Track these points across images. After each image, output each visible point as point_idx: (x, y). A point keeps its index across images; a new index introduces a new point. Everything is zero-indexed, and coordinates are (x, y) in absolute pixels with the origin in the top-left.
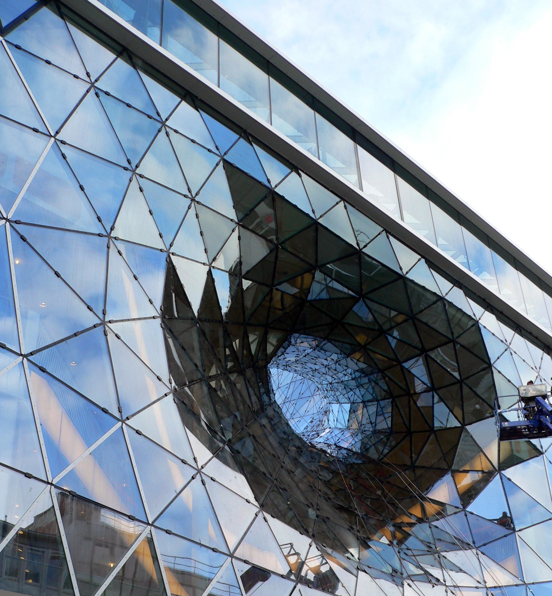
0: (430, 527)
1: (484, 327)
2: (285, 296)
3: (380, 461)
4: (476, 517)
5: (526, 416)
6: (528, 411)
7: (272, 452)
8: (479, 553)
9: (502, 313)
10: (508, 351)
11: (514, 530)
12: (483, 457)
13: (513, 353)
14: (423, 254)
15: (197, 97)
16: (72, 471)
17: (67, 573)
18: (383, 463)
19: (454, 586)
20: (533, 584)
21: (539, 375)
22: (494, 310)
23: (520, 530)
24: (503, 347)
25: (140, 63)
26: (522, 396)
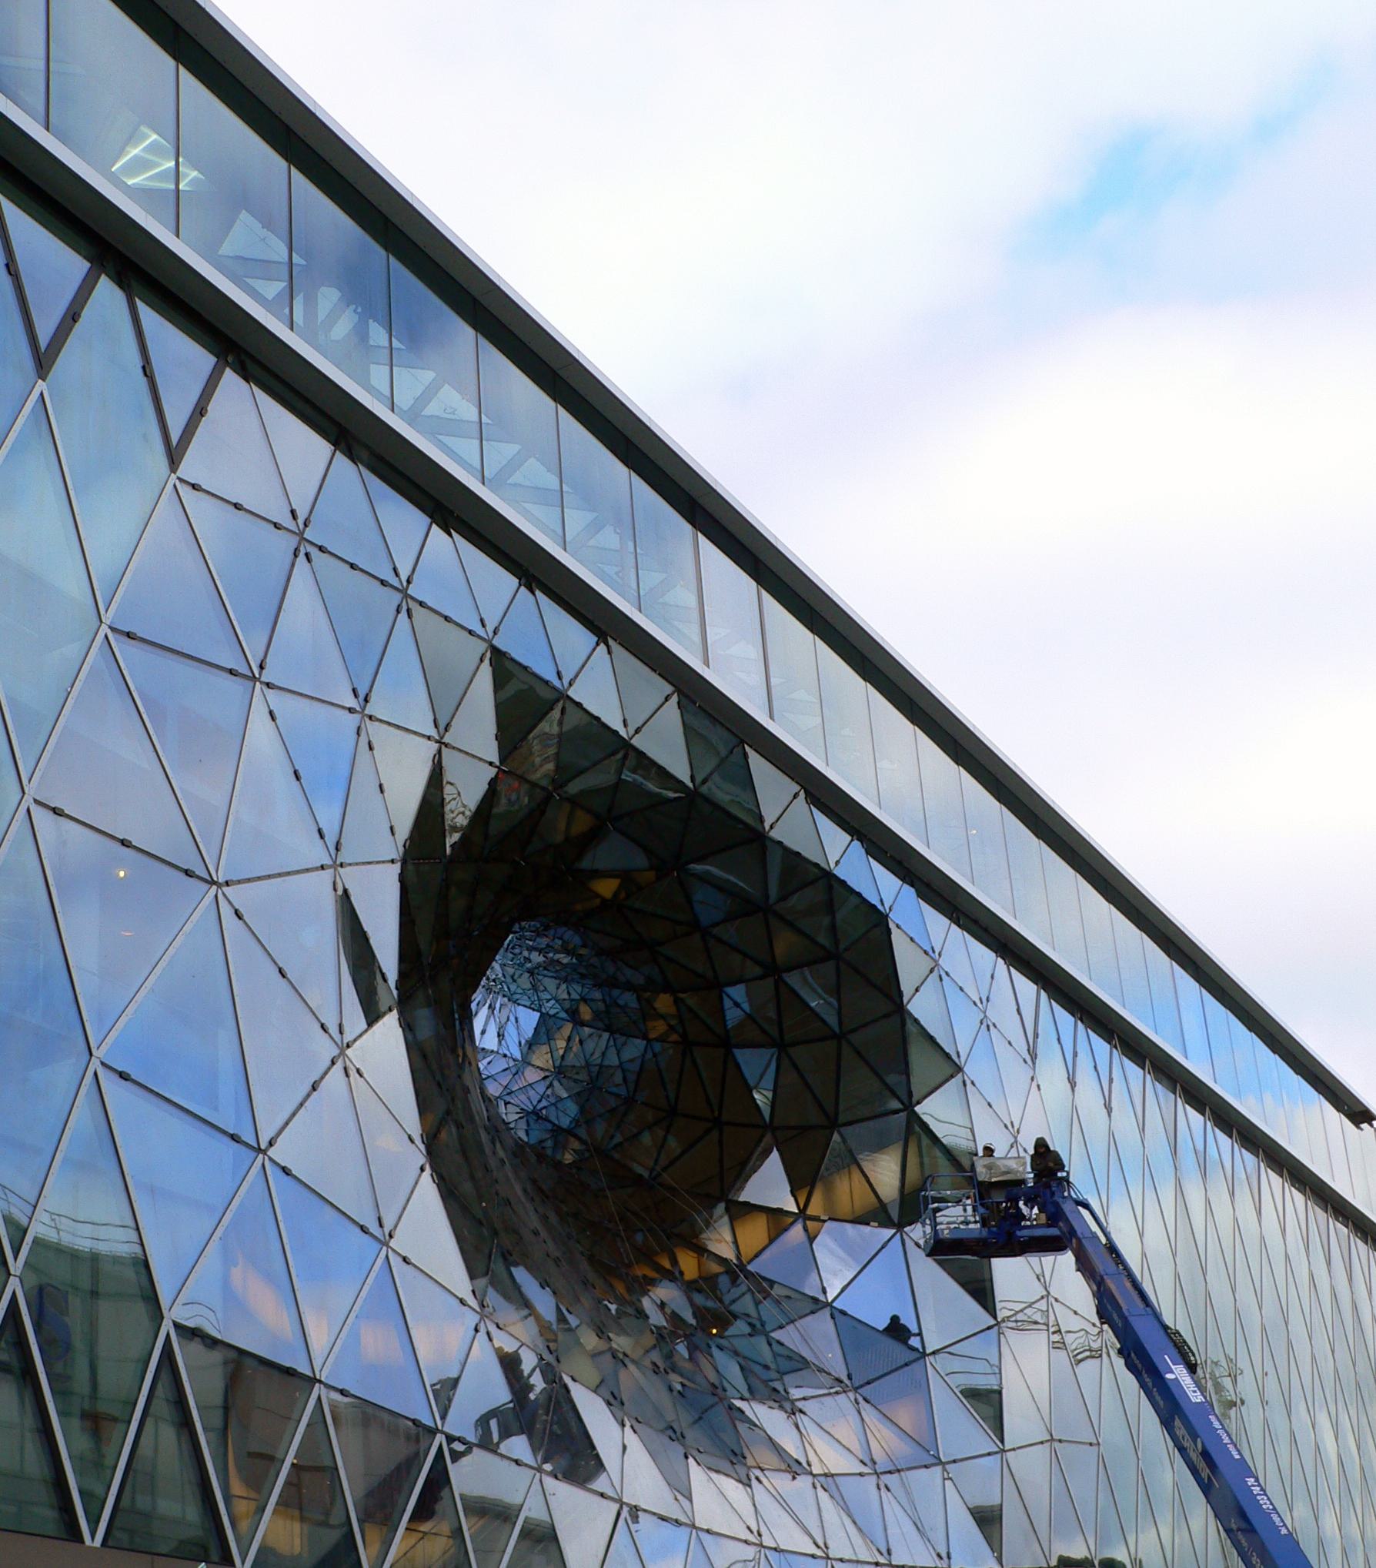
1: (898, 926)
3: (654, 1179)
5: (984, 1222)
8: (860, 1399)
9: (928, 885)
13: (968, 1083)
15: (452, 512)
16: (36, 1241)
17: (344, 1513)
18: (661, 1185)
19: (826, 1475)
24: (926, 963)
25: (365, 455)
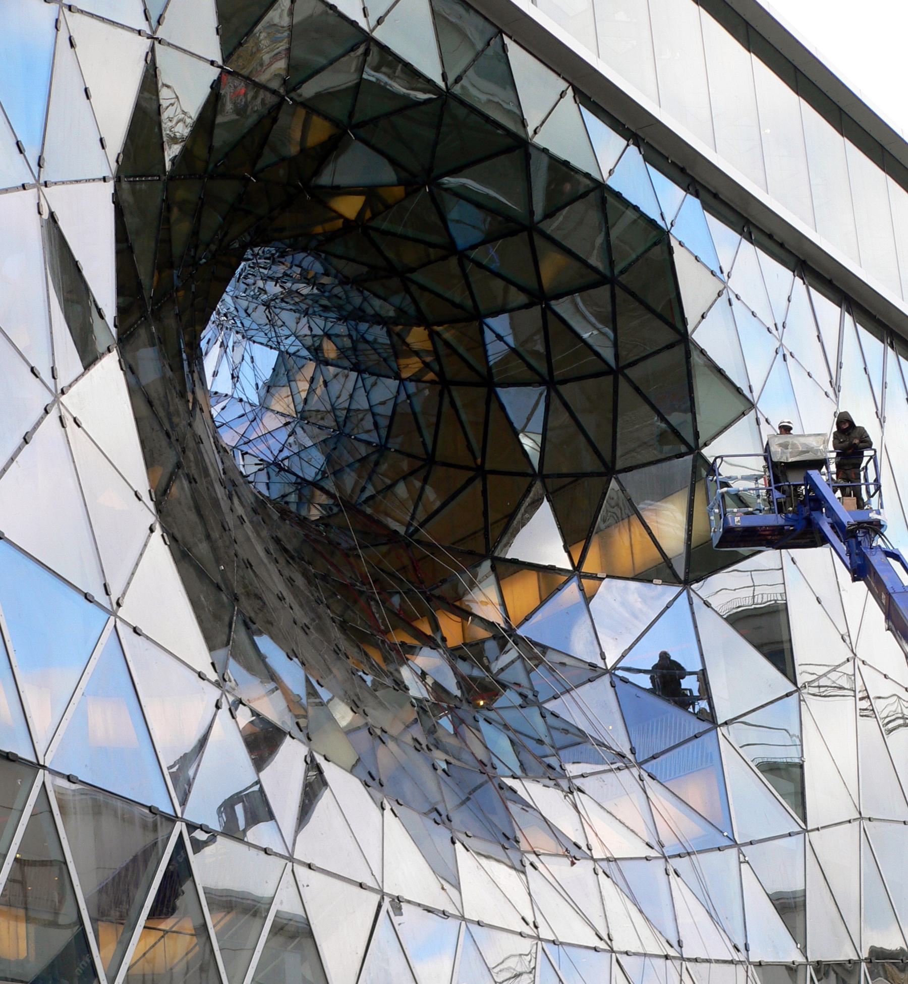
0: (543, 717)
2: (597, 582)
3: (411, 535)
4: (636, 691)
6: (784, 493)
7: (481, 754)
8: (645, 776)
9: (715, 196)
10: (724, 297)
11: (710, 717)
12: (637, 528)
14: (570, 80)
18: (419, 542)
19: (608, 860)
20: (751, 843)
21: (782, 345)
22: (701, 192)
23: (726, 723)
26: (775, 459)
